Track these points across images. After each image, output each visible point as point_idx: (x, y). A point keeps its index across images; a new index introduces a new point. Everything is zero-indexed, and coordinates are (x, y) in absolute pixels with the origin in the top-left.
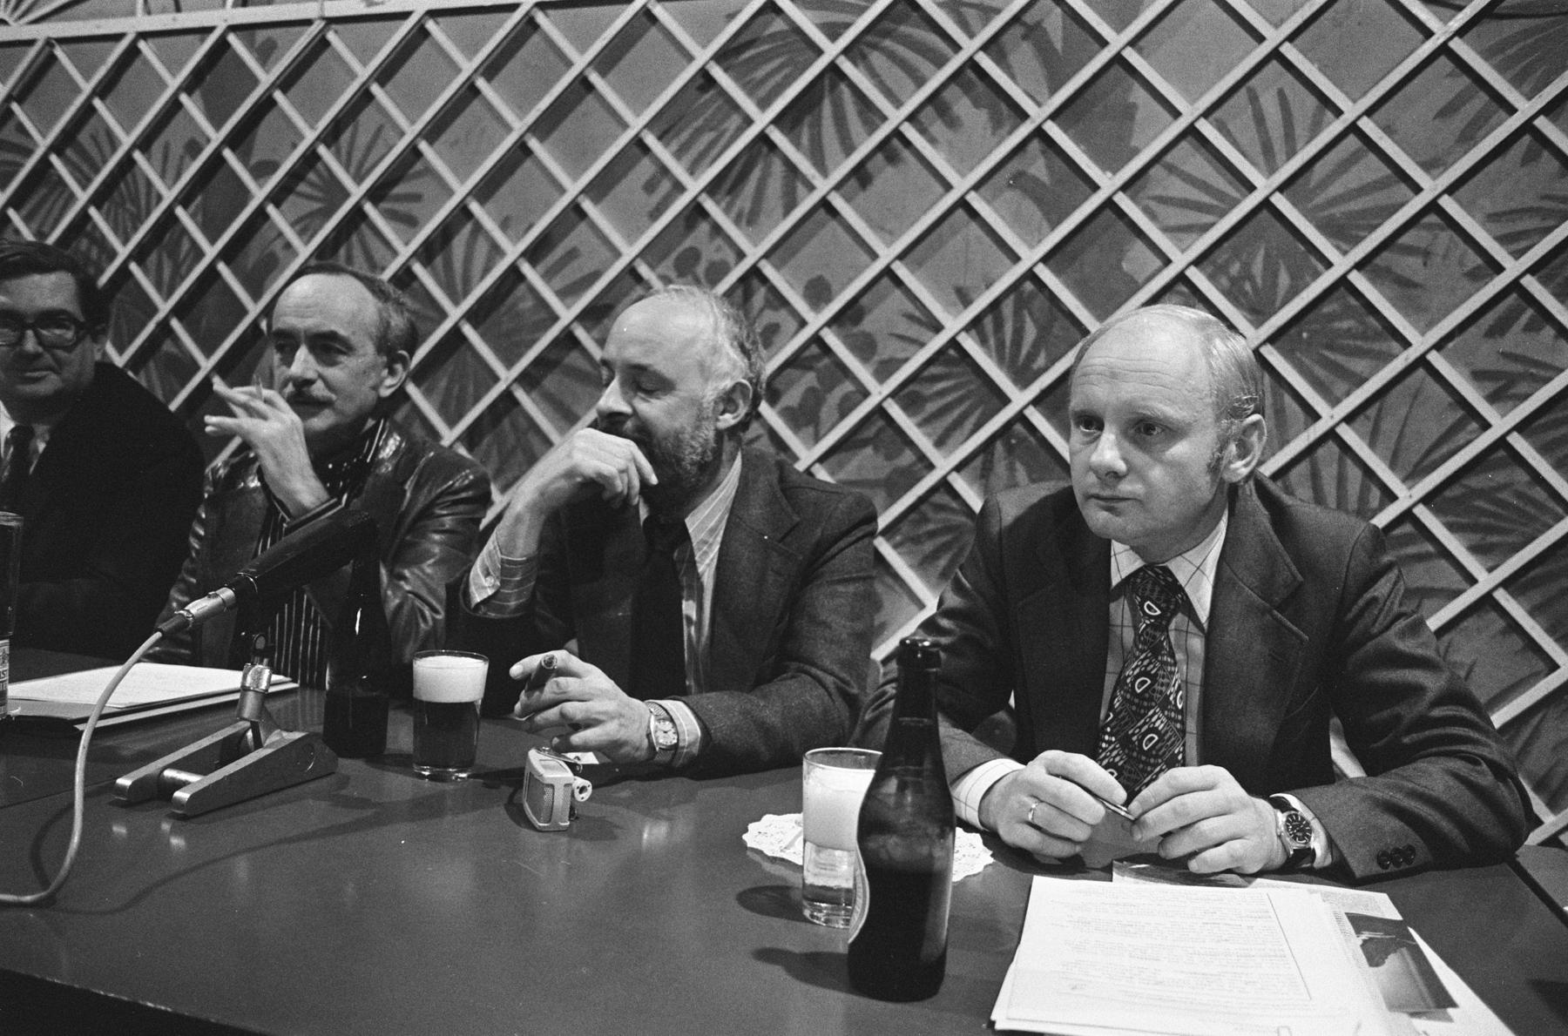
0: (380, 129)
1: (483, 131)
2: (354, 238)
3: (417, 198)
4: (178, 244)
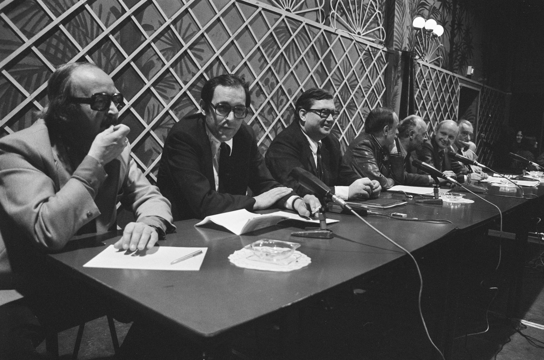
0: (190, 24)
1: (221, 34)
2: (183, 60)
3: (202, 51)
4: (109, 50)
